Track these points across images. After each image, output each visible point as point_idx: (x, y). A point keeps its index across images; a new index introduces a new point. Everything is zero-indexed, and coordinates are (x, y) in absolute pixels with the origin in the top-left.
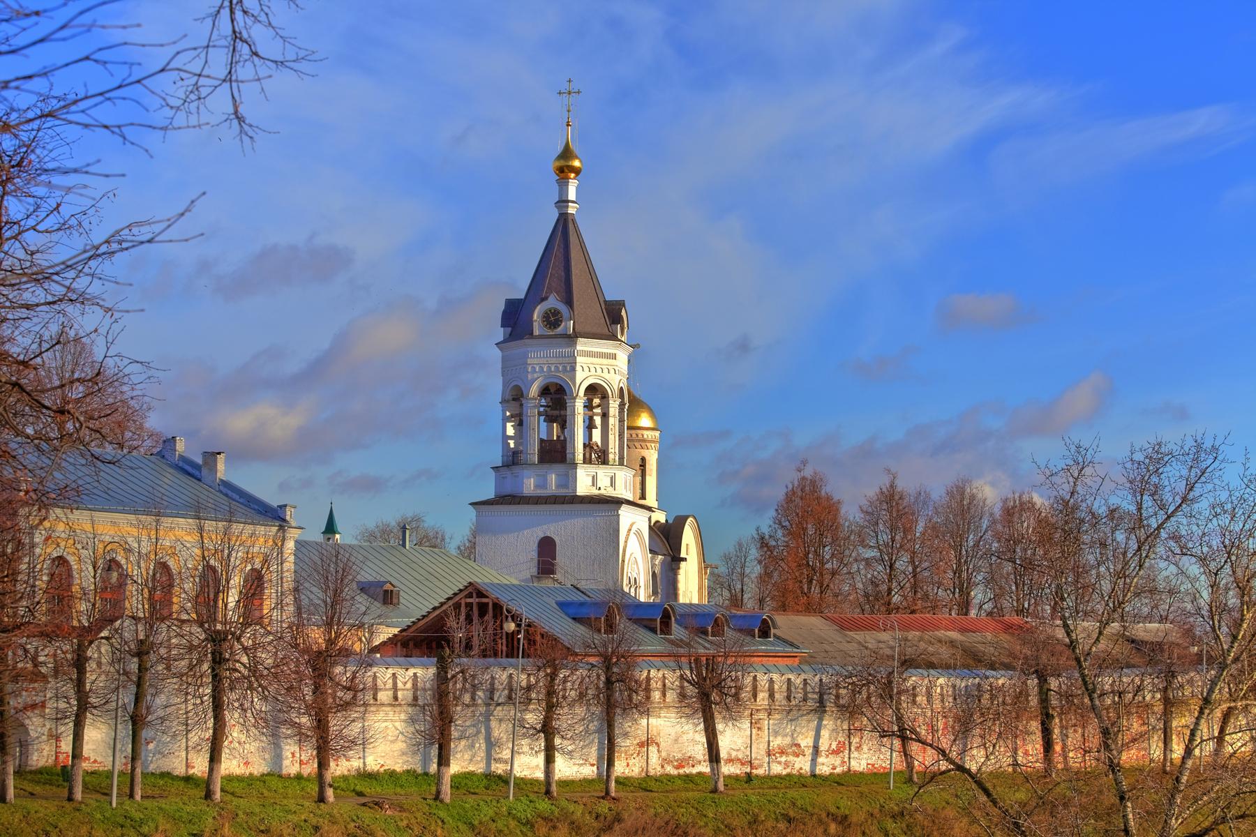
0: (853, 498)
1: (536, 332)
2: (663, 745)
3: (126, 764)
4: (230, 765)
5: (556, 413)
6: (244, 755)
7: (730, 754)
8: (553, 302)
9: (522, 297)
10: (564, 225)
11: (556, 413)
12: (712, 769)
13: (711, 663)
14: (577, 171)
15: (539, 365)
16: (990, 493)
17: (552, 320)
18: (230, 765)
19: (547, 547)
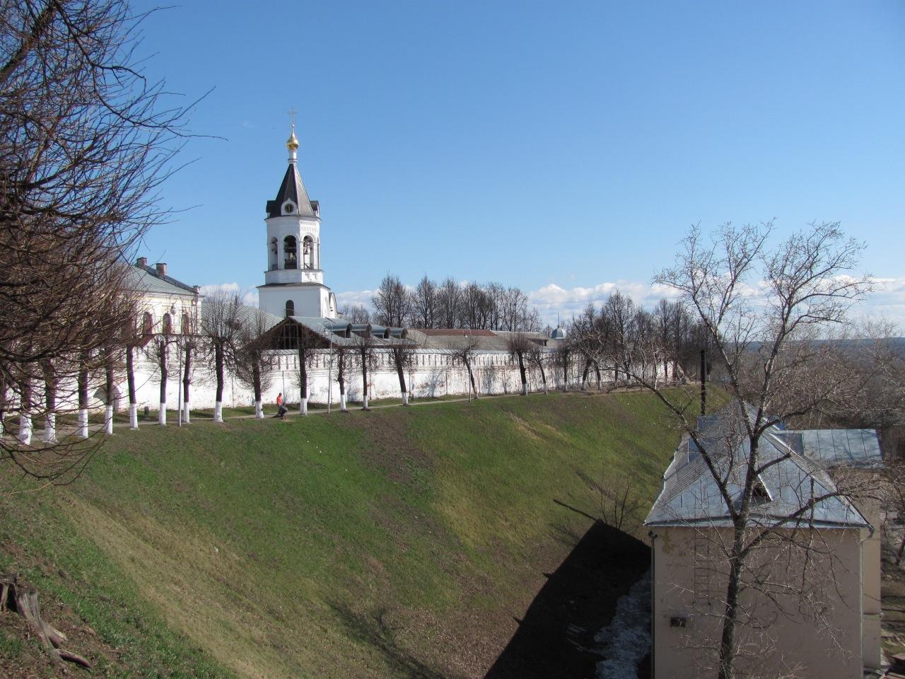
0: (410, 288)
1: (282, 214)
2: (376, 386)
3: (355, 379)
4: (227, 400)
5: (291, 248)
6: (202, 396)
7: (540, 382)
8: (289, 201)
9: (275, 199)
10: (290, 171)
11: (291, 248)
12: (403, 396)
13: (401, 347)
14: (296, 146)
15: (283, 227)
16: (463, 284)
17: (290, 208)
18: (227, 400)
19: (290, 305)
